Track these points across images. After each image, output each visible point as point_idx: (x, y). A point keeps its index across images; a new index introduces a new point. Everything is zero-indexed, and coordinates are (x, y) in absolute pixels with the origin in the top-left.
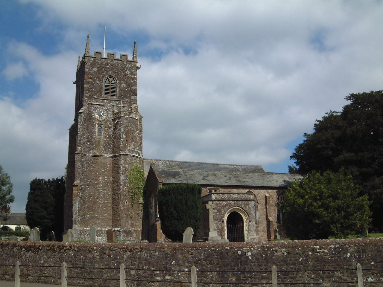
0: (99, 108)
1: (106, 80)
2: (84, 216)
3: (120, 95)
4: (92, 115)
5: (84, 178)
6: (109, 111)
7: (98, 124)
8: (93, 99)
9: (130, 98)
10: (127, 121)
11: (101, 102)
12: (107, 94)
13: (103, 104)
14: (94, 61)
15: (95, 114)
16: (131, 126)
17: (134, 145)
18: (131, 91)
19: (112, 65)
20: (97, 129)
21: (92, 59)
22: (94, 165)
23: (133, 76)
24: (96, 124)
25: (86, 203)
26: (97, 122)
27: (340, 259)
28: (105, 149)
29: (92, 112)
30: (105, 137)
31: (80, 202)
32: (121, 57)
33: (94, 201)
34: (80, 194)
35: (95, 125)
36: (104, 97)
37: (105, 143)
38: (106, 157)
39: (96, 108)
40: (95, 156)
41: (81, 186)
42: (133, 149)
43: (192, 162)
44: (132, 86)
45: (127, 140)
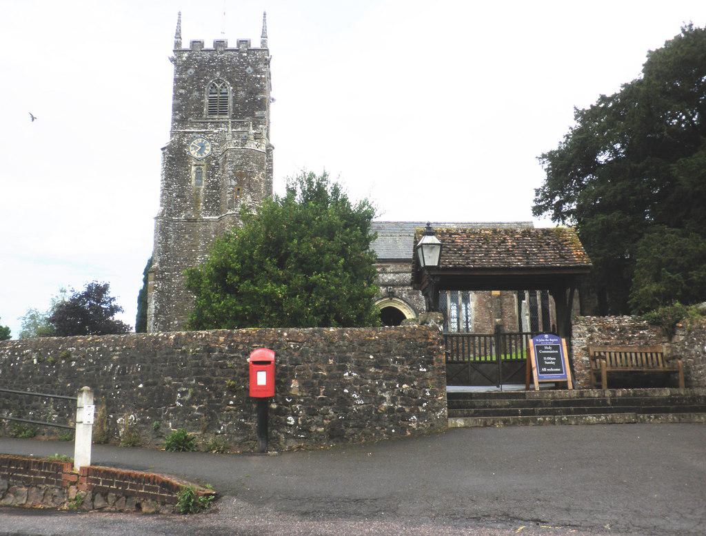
0: (197, 138)
1: (212, 88)
2: (169, 323)
3: (236, 110)
4: (185, 151)
5: (168, 259)
6: (216, 141)
7: (195, 165)
8: (186, 124)
9: (253, 115)
10: (240, 156)
11: (203, 128)
12: (212, 112)
13: (204, 130)
14: (189, 58)
15: (191, 148)
16: (247, 164)
17: (252, 197)
18: (255, 102)
19: (221, 61)
20: (193, 176)
21: (186, 55)
22: (187, 236)
23: (259, 76)
24: (191, 166)
25: (172, 301)
26: (194, 163)
27: (98, 375)
28: (207, 209)
29: (185, 146)
30: (208, 187)
31: (159, 300)
32: (238, 45)
33: (187, 298)
34: (159, 285)
35: (191, 168)
36: (206, 119)
37: (206, 197)
38: (208, 221)
39: (192, 139)
40: (189, 220)
41: (162, 272)
42: (249, 204)
43: (386, 223)
44: (257, 94)
45: (239, 190)
